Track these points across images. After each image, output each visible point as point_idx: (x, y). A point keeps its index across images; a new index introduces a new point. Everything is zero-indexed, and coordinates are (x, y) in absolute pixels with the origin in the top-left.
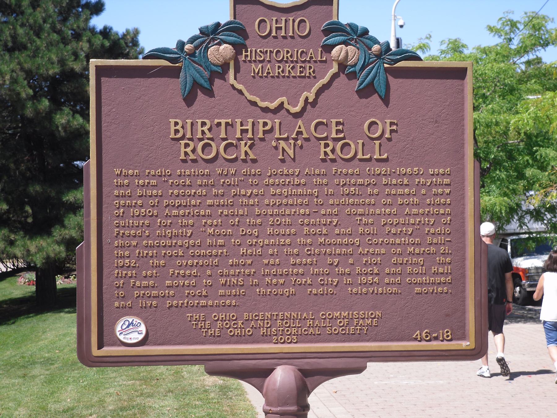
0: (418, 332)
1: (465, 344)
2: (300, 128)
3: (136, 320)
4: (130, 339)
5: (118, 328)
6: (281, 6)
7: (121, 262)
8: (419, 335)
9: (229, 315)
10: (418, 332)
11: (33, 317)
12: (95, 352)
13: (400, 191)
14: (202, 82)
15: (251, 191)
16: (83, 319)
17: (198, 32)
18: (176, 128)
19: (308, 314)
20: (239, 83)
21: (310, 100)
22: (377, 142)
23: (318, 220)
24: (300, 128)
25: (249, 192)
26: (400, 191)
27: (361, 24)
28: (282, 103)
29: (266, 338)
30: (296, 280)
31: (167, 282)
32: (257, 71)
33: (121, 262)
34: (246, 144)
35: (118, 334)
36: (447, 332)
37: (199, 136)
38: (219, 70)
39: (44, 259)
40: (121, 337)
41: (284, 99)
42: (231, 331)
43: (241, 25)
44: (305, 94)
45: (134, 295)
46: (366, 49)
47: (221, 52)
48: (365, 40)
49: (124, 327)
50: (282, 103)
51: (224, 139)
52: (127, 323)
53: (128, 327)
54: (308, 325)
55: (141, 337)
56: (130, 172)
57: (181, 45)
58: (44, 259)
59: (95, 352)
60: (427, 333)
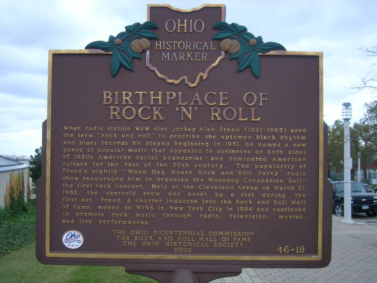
0: (280, 248)
1: (313, 258)
2: (196, 98)
3: (77, 233)
4: (73, 246)
5: (64, 238)
6: (182, 11)
7: (67, 192)
8: (281, 249)
9: (143, 232)
10: (280, 248)
11: (5, 202)
12: (49, 254)
13: (269, 145)
14: (126, 64)
15: (160, 143)
16: (30, 186)
17: (124, 30)
18: (107, 97)
19: (200, 233)
20: (153, 66)
21: (204, 78)
22: (253, 109)
23: (209, 165)
24: (196, 98)
25: (159, 144)
26: (269, 145)
27: (240, 23)
28: (184, 80)
29: (170, 250)
30: (191, 208)
31: (99, 207)
32: (166, 57)
33: (67, 192)
34: (157, 109)
35: (64, 242)
36: (302, 248)
37: (124, 103)
38: (138, 56)
39: (11, 156)
40: (66, 244)
41: (185, 77)
42: (144, 243)
43: (155, 25)
44: (201, 74)
45: (76, 216)
46: (246, 42)
47: (138, 44)
48: (245, 36)
49: (68, 237)
50: (184, 80)
51: (141, 106)
52: (70, 235)
53: (71, 237)
54: (200, 241)
55: (80, 245)
56: (75, 128)
57: (112, 38)
58: (11, 156)
59: (49, 254)
60: (287, 248)
